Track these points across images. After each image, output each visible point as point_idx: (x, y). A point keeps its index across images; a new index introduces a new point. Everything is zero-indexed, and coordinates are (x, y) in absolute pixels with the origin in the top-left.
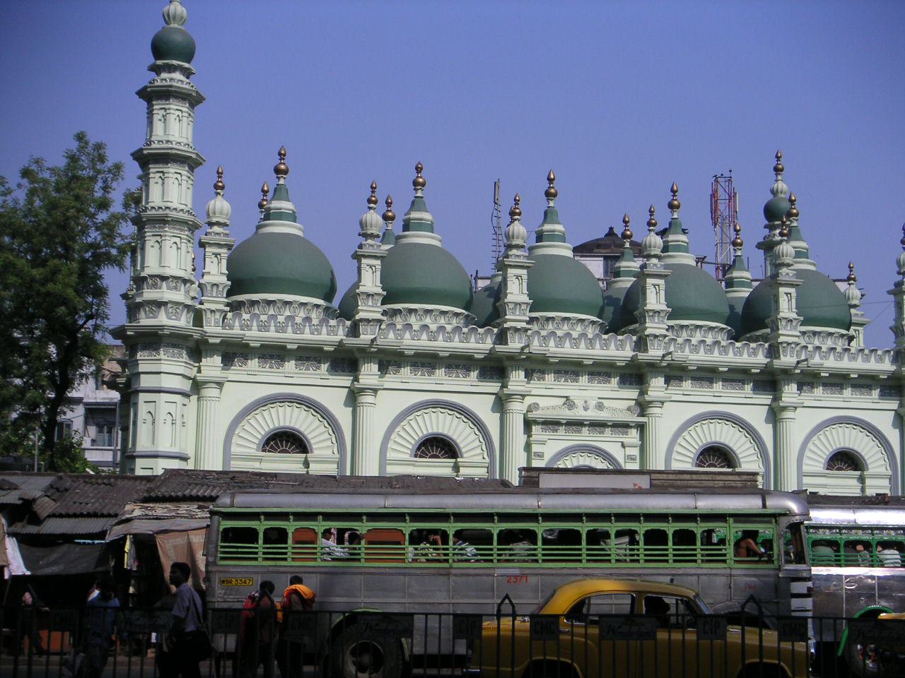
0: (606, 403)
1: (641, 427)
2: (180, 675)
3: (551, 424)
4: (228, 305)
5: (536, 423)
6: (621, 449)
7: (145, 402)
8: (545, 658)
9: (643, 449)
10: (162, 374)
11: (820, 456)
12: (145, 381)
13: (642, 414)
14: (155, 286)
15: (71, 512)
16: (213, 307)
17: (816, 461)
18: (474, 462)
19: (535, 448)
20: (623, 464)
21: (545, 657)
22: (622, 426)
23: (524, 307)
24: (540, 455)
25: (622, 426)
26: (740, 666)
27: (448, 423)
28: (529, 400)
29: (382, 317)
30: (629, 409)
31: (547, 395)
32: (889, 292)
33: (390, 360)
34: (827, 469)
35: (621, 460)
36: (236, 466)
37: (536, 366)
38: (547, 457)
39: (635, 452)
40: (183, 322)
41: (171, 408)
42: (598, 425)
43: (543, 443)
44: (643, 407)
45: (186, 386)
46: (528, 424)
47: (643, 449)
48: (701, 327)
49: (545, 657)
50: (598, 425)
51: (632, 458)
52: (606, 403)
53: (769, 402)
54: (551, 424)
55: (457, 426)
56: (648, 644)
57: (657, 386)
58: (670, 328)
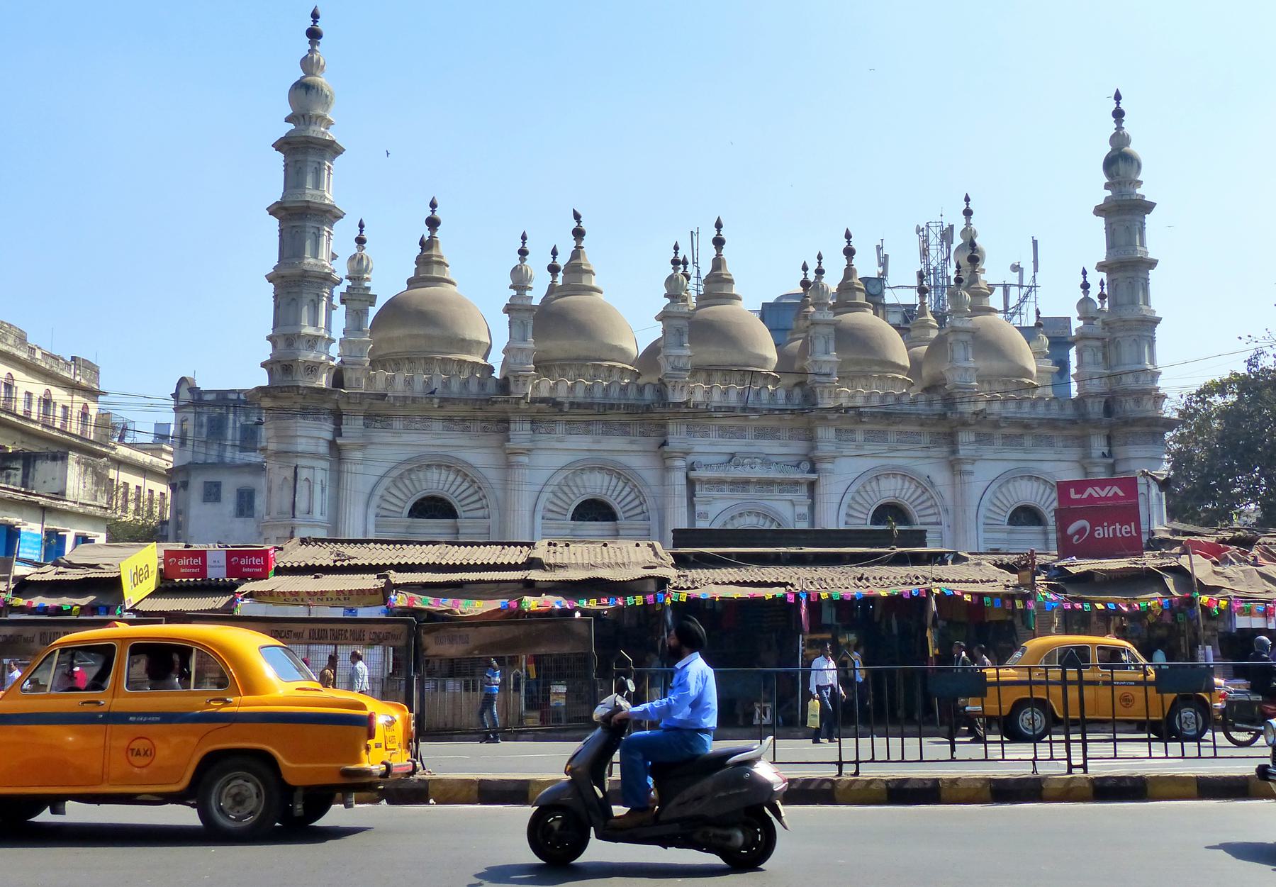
1: (812, 486)
2: (1138, 191)
6: (788, 511)
7: (1120, 163)
9: (812, 508)
13: (813, 470)
19: (699, 508)
28: (691, 458)
31: (708, 448)
36: (701, 524)
38: (711, 517)
39: (804, 510)
43: (708, 503)
46: (691, 483)
47: (812, 508)
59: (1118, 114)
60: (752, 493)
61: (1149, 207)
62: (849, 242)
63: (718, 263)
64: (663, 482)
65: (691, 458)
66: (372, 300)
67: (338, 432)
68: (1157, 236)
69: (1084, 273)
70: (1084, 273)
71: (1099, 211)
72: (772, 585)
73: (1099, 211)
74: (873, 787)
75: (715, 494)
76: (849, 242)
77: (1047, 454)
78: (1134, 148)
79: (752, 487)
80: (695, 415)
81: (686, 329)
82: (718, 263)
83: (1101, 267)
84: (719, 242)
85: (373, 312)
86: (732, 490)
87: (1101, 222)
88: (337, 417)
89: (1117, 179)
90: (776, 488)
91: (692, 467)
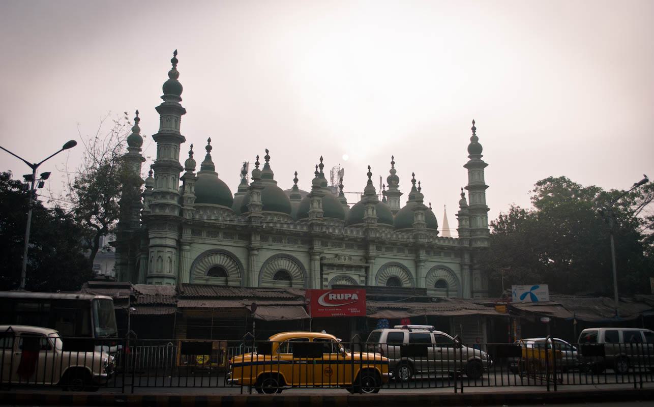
0: (353, 257)
3: (331, 266)
4: (194, 207)
5: (325, 265)
8: (36, 383)
9: (366, 278)
10: (167, 239)
11: (202, 270)
13: (367, 263)
15: (470, 308)
16: (188, 208)
17: (203, 268)
18: (234, 279)
19: (324, 276)
20: (359, 283)
21: (52, 383)
22: (359, 268)
23: (321, 214)
24: (327, 279)
25: (359, 268)
26: (359, 369)
27: (395, 270)
28: (322, 255)
29: (262, 216)
30: (361, 260)
31: (330, 253)
32: (456, 215)
34: (274, 279)
35: (358, 282)
39: (363, 279)
40: (176, 213)
41: (169, 255)
42: (349, 267)
43: (328, 274)
44: (367, 258)
46: (322, 265)
47: (366, 278)
48: (277, 214)
49: (52, 383)
50: (349, 267)
51: (362, 281)
52: (353, 257)
53: (306, 250)
54: (331, 266)
55: (291, 265)
56: (458, 350)
58: (263, 214)
59: (474, 129)
60: (345, 272)
61: (183, 111)
62: (369, 170)
63: (208, 157)
64: (462, 276)
65: (322, 255)
67: (180, 236)
68: (489, 176)
69: (258, 157)
70: (258, 157)
71: (465, 166)
72: (241, 298)
73: (465, 166)
74: (414, 386)
75: (330, 271)
76: (369, 170)
78: (180, 80)
79: (353, 269)
80: (381, 244)
81: (321, 201)
82: (208, 157)
83: (466, 188)
84: (209, 148)
86: (337, 269)
87: (466, 170)
88: (180, 231)
90: (335, 268)
91: (322, 259)
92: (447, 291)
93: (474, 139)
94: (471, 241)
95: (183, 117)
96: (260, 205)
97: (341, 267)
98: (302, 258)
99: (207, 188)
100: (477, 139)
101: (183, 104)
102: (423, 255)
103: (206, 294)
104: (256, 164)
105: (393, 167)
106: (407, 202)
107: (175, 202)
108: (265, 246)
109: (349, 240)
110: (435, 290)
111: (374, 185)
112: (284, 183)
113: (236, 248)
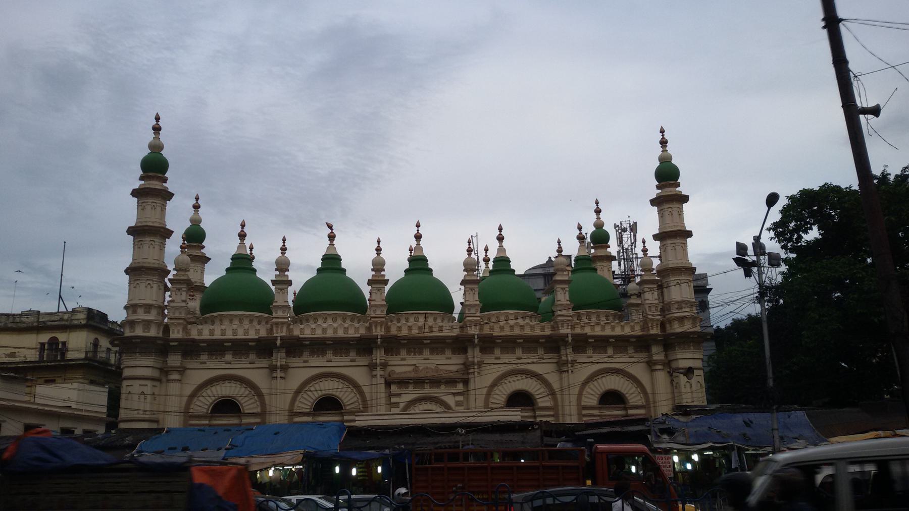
3: (403, 382)
12: (126, 373)
14: (680, 308)
17: (591, 399)
28: (390, 369)
33: (581, 343)
37: (393, 344)
40: (153, 332)
43: (399, 395)
45: (156, 374)
46: (388, 384)
54: (403, 382)
57: (474, 355)
61: (685, 199)
63: (501, 249)
66: (386, 282)
71: (654, 202)
75: (403, 391)
77: (533, 358)
82: (501, 249)
85: (387, 288)
89: (155, 184)
92: (534, 410)
93: (156, 148)
94: (663, 326)
95: (169, 204)
96: (476, 305)
97: (419, 382)
98: (639, 371)
99: (242, 289)
100: (161, 147)
101: (170, 186)
102: (568, 354)
103: (497, 437)
104: (377, 250)
105: (598, 218)
106: (227, 270)
107: (152, 316)
108: (581, 358)
109: (503, 342)
110: (600, 409)
111: (210, 247)
112: (357, 266)
113: (545, 367)
